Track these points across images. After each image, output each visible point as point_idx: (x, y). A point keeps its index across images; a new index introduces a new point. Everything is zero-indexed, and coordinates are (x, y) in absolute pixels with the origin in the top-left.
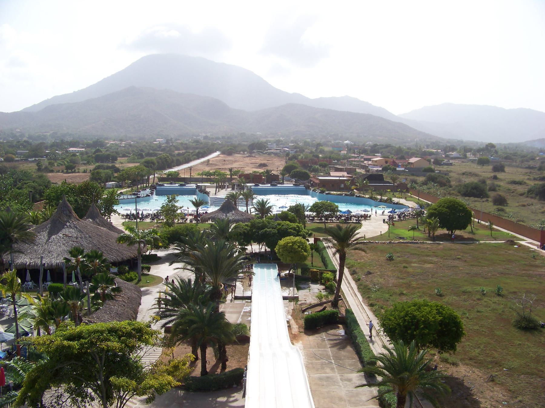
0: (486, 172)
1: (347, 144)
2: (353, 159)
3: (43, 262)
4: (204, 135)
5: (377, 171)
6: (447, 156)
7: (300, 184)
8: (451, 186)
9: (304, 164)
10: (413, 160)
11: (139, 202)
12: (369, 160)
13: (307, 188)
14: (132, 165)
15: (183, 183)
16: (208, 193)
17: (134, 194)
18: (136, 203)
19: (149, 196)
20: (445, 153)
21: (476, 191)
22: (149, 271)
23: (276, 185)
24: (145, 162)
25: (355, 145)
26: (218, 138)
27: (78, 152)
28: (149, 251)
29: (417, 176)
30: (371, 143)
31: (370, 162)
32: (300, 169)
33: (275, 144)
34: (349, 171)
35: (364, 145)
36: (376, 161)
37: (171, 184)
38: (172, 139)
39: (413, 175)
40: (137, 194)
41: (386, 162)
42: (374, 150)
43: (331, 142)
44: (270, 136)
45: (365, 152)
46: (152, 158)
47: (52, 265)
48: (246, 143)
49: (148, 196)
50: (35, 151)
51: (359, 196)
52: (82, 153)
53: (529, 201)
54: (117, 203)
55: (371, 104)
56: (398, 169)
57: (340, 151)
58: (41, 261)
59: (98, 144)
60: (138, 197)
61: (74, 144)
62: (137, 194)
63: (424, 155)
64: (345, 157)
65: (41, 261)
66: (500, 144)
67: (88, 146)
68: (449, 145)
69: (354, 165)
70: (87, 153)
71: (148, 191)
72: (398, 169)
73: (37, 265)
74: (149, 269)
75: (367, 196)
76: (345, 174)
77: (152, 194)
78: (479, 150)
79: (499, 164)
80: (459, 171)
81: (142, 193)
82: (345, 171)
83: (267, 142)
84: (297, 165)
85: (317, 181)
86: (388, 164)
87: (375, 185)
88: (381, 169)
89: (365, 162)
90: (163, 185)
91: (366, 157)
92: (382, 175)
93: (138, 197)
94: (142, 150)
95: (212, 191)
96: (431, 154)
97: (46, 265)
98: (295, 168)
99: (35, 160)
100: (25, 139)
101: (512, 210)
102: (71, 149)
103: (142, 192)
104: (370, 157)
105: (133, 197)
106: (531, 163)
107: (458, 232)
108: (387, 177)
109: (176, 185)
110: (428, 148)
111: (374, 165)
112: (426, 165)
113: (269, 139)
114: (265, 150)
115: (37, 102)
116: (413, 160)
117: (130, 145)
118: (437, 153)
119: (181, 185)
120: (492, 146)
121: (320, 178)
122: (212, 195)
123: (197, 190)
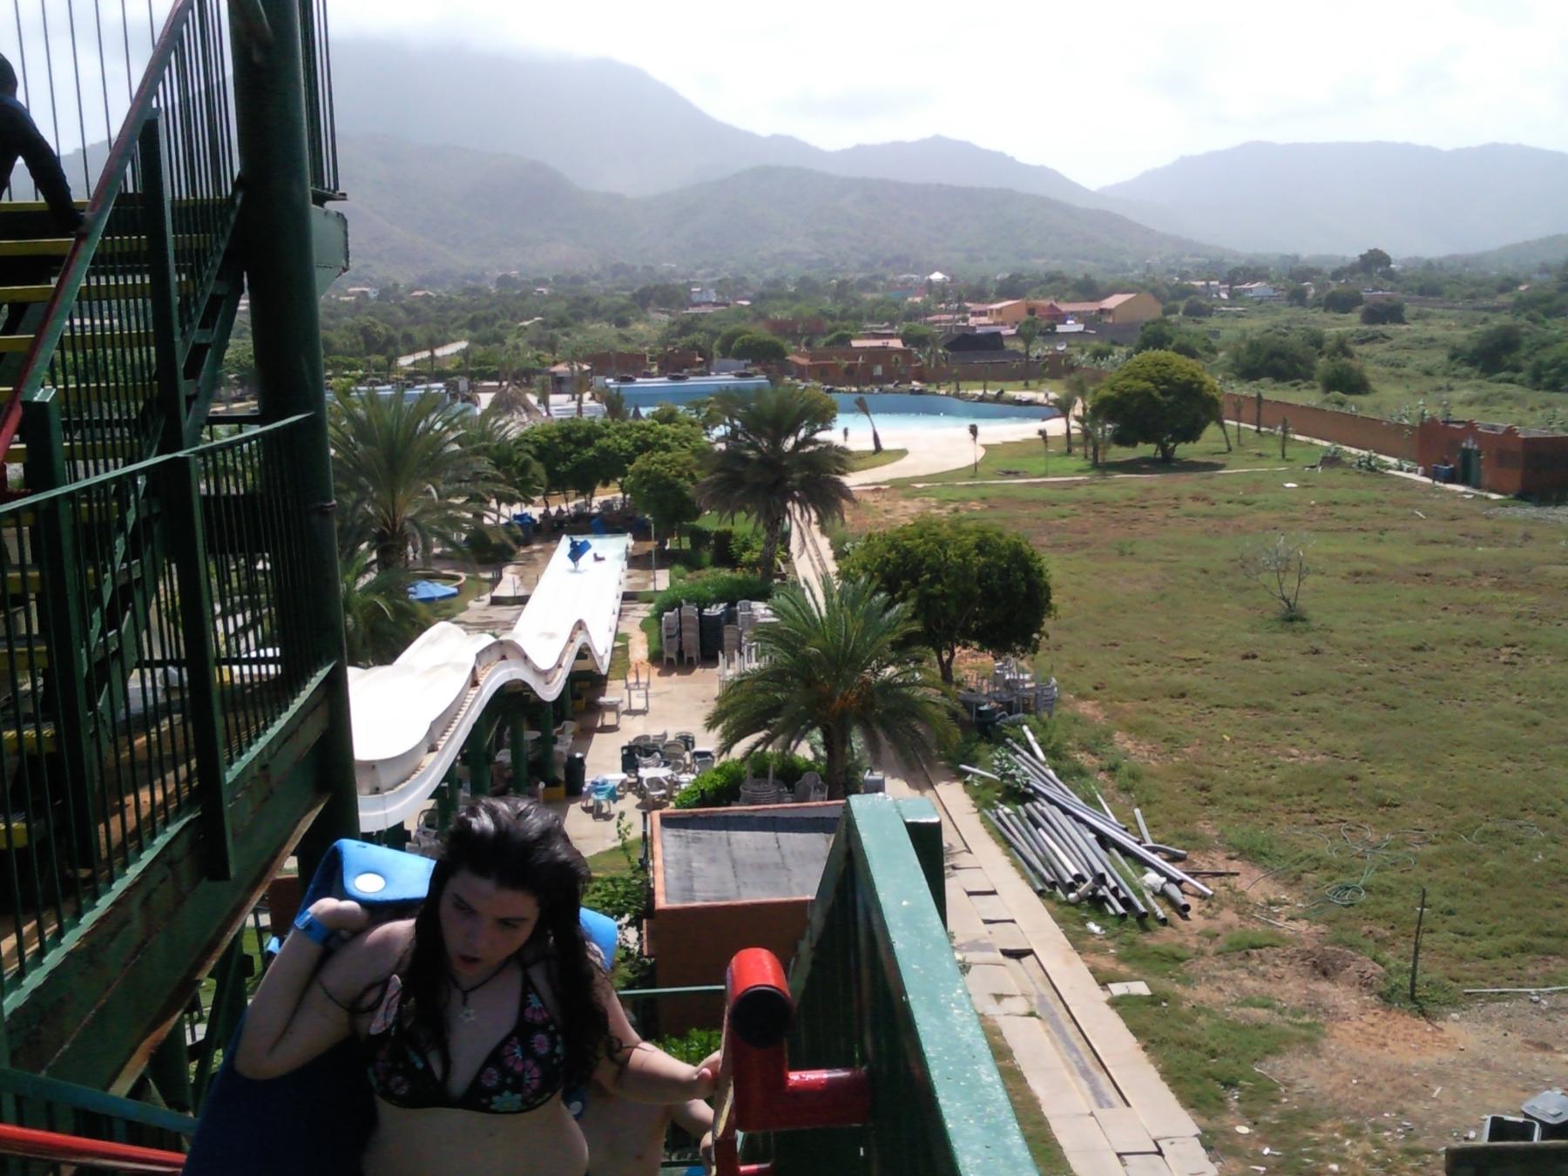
0: (1336, 326)
7: (756, 373)
10: (1112, 302)
41: (1031, 311)
44: (700, 272)
55: (1012, 159)
56: (1060, 328)
72: (1060, 328)
75: (943, 392)
78: (1336, 275)
83: (690, 284)
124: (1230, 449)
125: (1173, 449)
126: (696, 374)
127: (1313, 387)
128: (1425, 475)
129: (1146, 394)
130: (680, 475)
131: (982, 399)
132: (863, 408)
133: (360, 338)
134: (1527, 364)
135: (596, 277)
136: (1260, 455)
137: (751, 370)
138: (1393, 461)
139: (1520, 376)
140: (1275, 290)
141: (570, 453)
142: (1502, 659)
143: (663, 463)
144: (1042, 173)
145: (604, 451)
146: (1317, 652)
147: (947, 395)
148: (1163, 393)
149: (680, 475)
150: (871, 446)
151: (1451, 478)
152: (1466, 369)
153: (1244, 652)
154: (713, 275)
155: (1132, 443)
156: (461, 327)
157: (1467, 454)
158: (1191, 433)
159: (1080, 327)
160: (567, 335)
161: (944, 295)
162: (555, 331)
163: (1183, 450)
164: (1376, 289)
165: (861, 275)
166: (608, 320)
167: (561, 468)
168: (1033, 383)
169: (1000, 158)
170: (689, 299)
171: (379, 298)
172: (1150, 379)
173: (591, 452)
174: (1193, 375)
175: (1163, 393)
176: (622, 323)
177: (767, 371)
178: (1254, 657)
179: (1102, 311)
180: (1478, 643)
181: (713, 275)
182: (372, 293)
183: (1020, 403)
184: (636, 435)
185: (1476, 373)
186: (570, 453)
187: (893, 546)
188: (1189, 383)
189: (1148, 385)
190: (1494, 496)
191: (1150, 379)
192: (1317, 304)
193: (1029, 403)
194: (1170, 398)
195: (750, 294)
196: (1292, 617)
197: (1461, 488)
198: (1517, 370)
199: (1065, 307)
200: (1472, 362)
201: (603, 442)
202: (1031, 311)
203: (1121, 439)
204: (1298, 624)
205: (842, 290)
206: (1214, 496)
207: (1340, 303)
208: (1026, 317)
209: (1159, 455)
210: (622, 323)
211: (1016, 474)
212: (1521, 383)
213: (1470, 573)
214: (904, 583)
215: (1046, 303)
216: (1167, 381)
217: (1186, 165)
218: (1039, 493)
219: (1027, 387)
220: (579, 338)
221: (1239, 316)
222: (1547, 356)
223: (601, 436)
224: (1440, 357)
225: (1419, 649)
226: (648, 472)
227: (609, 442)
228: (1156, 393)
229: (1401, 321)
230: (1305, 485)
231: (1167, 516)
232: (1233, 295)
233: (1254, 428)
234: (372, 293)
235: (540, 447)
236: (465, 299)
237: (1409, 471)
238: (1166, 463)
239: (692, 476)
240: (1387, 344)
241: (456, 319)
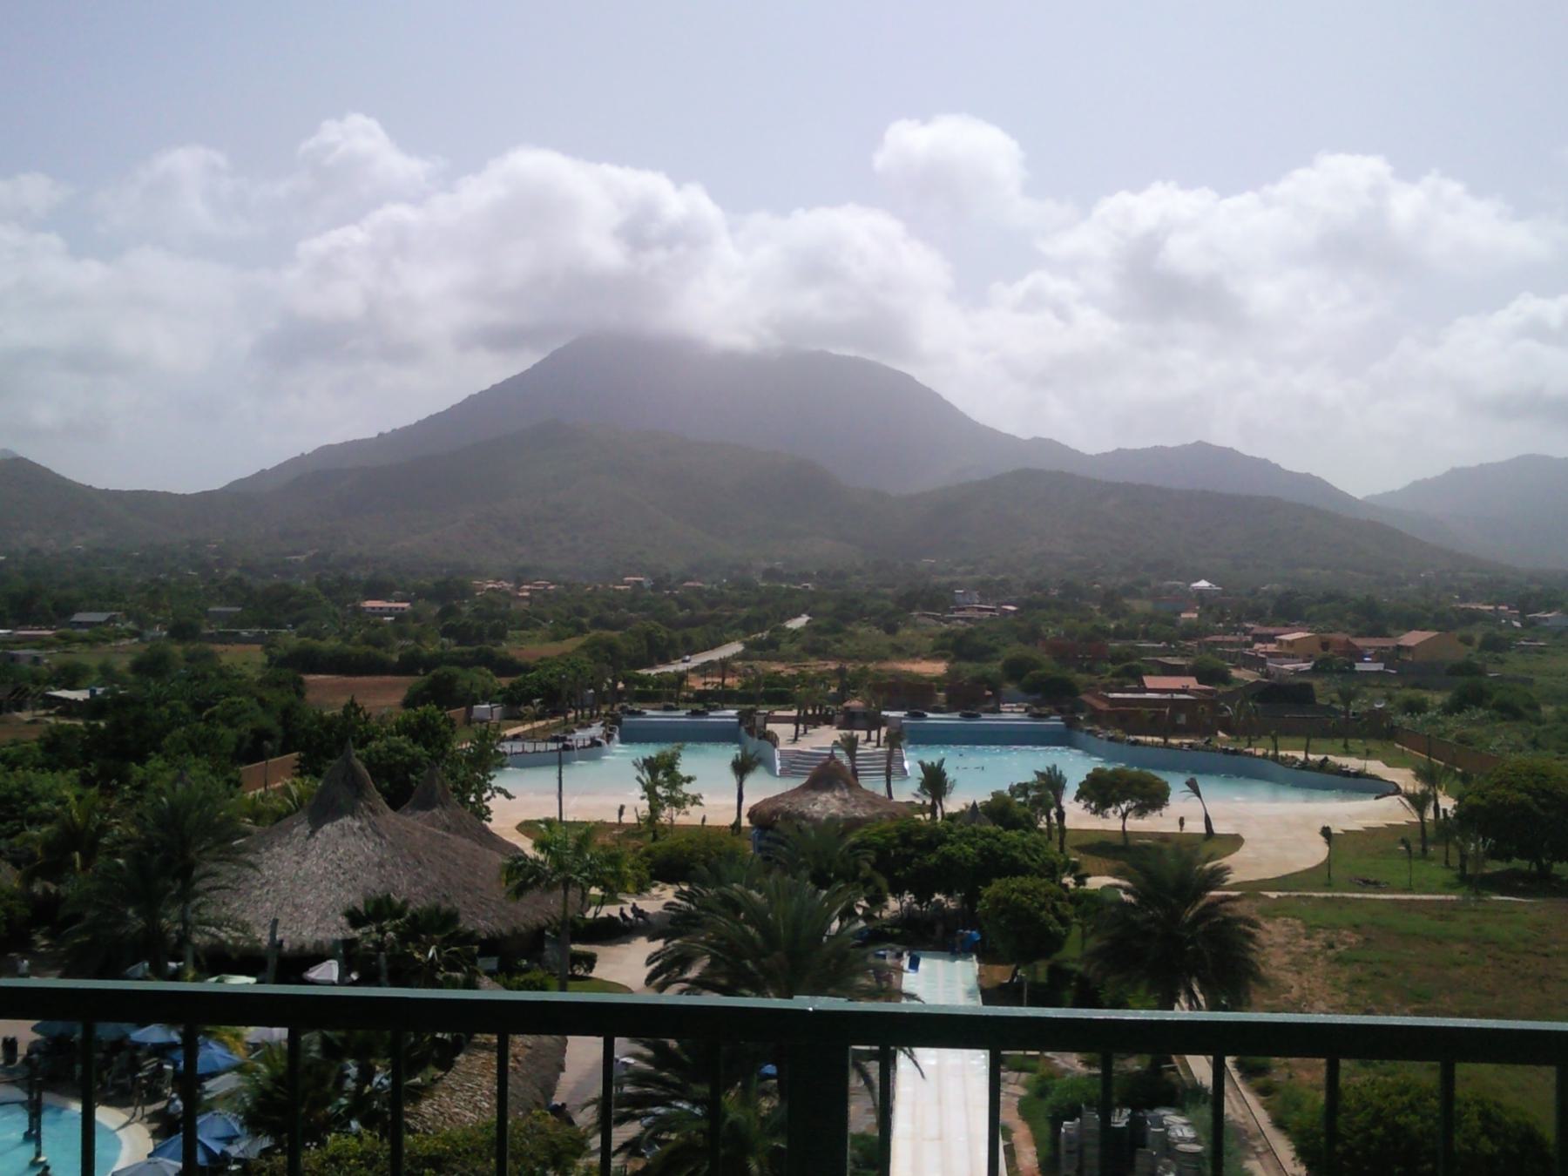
1: (1201, 591)
2: (1219, 638)
3: (278, 937)
4: (765, 565)
5: (1296, 671)
6: (1529, 624)
7: (1051, 714)
9: (1062, 653)
10: (1412, 638)
11: (568, 762)
12: (1270, 639)
13: (1071, 724)
14: (552, 649)
15: (700, 707)
16: (772, 739)
17: (556, 740)
18: (560, 764)
19: (599, 744)
22: (591, 968)
23: (976, 716)
25: (1223, 593)
26: (806, 577)
27: (390, 612)
28: (593, 909)
29: (1426, 688)
30: (1276, 586)
31: (1271, 647)
32: (1049, 667)
33: (975, 594)
34: (1203, 675)
35: (1254, 592)
36: (1291, 644)
37: (667, 708)
38: (668, 575)
39: (1416, 686)
40: (564, 739)
41: (1325, 646)
42: (1288, 610)
43: (1147, 584)
44: (960, 569)
45: (1257, 615)
46: (615, 634)
47: (302, 947)
48: (889, 591)
49: (595, 743)
50: (270, 606)
51: (1235, 752)
52: (400, 617)
54: (501, 762)
55: (1277, 466)
56: (1359, 667)
57: (1178, 614)
58: (273, 934)
59: (448, 592)
60: (566, 748)
61: (377, 589)
62: (564, 739)
63: (1441, 621)
64: (1191, 632)
65: (273, 934)
67: (422, 593)
68: (1536, 588)
69: (1223, 656)
70: (417, 617)
71: (596, 730)
72: (1359, 667)
73: (258, 949)
74: (590, 961)
75: (1259, 752)
76: (1192, 682)
77: (609, 738)
81: (581, 736)
82: (1191, 674)
83: (953, 585)
84: (1038, 653)
85: (1104, 706)
86: (1330, 652)
87: (1276, 721)
88: (1307, 666)
89: (1258, 646)
90: (640, 714)
91: (1258, 629)
92: (1309, 687)
93: (566, 748)
94: (581, 612)
95: (783, 731)
96: (1473, 617)
97: (286, 945)
98: (1036, 665)
99: (261, 635)
100: (233, 572)
102: (369, 604)
103: (579, 733)
104: (1271, 630)
105: (553, 746)
107: (987, 719)
108: (1325, 691)
109: (681, 716)
110: (1464, 599)
111: (1287, 656)
113: (957, 578)
114: (947, 610)
115: (269, 464)
116: (1412, 638)
117: (546, 595)
119: (695, 713)
121: (1111, 695)
122: (784, 745)
123: (743, 729)
126: (987, 711)
130: (1042, 907)
131: (1305, 765)
133: (645, 643)
135: (859, 572)
137: (1045, 710)
141: (912, 857)
143: (1024, 892)
144: (1309, 481)
145: (947, 859)
147: (1265, 756)
148: (1543, 806)
149: (1042, 907)
150: (1203, 831)
154: (972, 573)
155: (1507, 857)
156: (734, 627)
160: (839, 641)
161: (1223, 614)
162: (828, 638)
165: (1124, 580)
166: (877, 624)
167: (900, 873)
168: (1355, 744)
169: (1263, 464)
170: (954, 603)
171: (653, 588)
173: (932, 859)
175: (1543, 806)
176: (891, 630)
177: (1060, 711)
179: (1399, 648)
181: (972, 573)
182: (647, 582)
183: (1348, 774)
184: (982, 843)
186: (912, 857)
189: (1524, 796)
193: (1359, 775)
195: (1013, 598)
201: (946, 848)
202: (1325, 646)
205: (1110, 601)
208: (1321, 654)
210: (891, 630)
211: (1376, 886)
220: (851, 645)
223: (943, 841)
226: (1006, 901)
227: (953, 849)
228: (1535, 807)
232: (1529, 624)
234: (647, 582)
235: (882, 852)
236: (736, 594)
239: (1054, 908)
241: (730, 618)
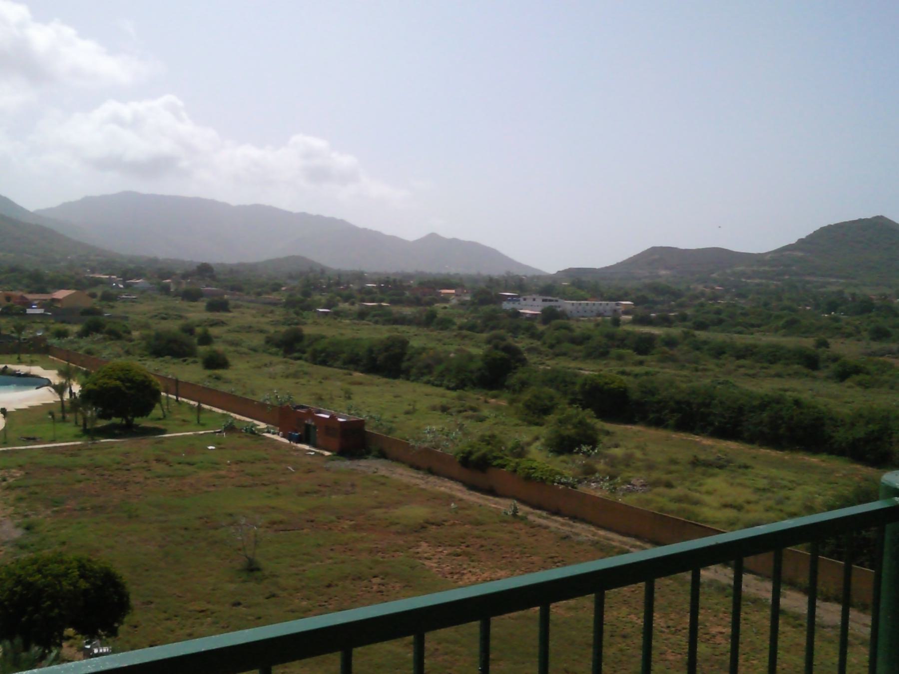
0: (197, 313)
8: (131, 340)
20: (124, 280)
21: (170, 347)
24: (67, 336)
29: (69, 323)
39: (63, 322)
53: (266, 358)
56: (29, 311)
63: (78, 284)
66: (222, 265)
68: (132, 266)
72: (29, 311)
78: (185, 276)
79: (216, 298)
80: (141, 312)
86: (11, 303)
96: (98, 282)
101: (242, 374)
106: (274, 296)
107: (138, 421)
110: (93, 271)
112: (87, 303)
116: (61, 294)
118: (109, 283)
120: (362, 273)
124: (165, 416)
125: (133, 420)
127: (195, 362)
128: (284, 436)
129: (117, 388)
132: (121, 623)
134: (309, 350)
136: (184, 421)
138: (262, 425)
139: (305, 356)
140: (151, 284)
142: (375, 587)
146: (274, 596)
151: (299, 440)
152: (274, 350)
153: (233, 601)
157: (308, 427)
158: (145, 410)
159: (41, 311)
163: (142, 422)
164: (207, 286)
168: (25, 357)
172: (119, 379)
174: (146, 377)
175: (128, 388)
178: (239, 604)
180: (359, 578)
183: (19, 375)
185: (281, 352)
187: (19, 581)
188: (143, 382)
189: (118, 383)
190: (327, 453)
191: (119, 379)
192: (176, 295)
194: (132, 392)
196: (252, 568)
197: (307, 447)
198: (304, 352)
199: (30, 297)
200: (278, 345)
202: (8, 298)
203: (102, 416)
204: (258, 574)
206: (170, 458)
207: (191, 296)
209: (124, 422)
212: (306, 360)
213: (333, 518)
214: (30, 609)
215: (18, 293)
216: (131, 381)
217: (88, 202)
218: (57, 459)
219: (20, 362)
221: (133, 301)
222: (319, 347)
224: (258, 340)
225: (329, 586)
228: (123, 389)
229: (228, 311)
230: (220, 447)
231: (146, 478)
232: (127, 286)
233: (175, 397)
237: (274, 434)
238: (128, 431)
240: (226, 328)
